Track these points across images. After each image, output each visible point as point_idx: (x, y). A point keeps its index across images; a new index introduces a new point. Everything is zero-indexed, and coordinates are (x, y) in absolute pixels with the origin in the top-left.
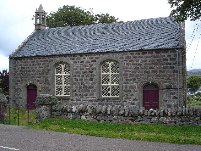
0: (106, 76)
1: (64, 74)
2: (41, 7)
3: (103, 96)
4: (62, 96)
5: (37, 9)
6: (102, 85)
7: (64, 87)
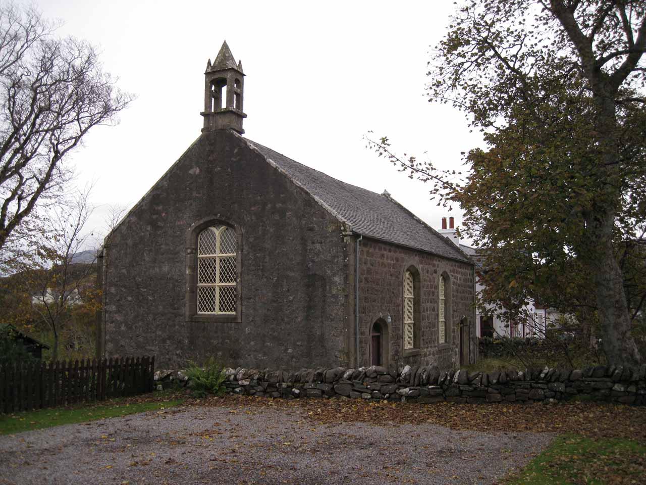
0: (228, 260)
1: (221, 255)
2: (225, 51)
3: (200, 313)
4: (213, 313)
5: (209, 63)
6: (200, 284)
7: (220, 290)
